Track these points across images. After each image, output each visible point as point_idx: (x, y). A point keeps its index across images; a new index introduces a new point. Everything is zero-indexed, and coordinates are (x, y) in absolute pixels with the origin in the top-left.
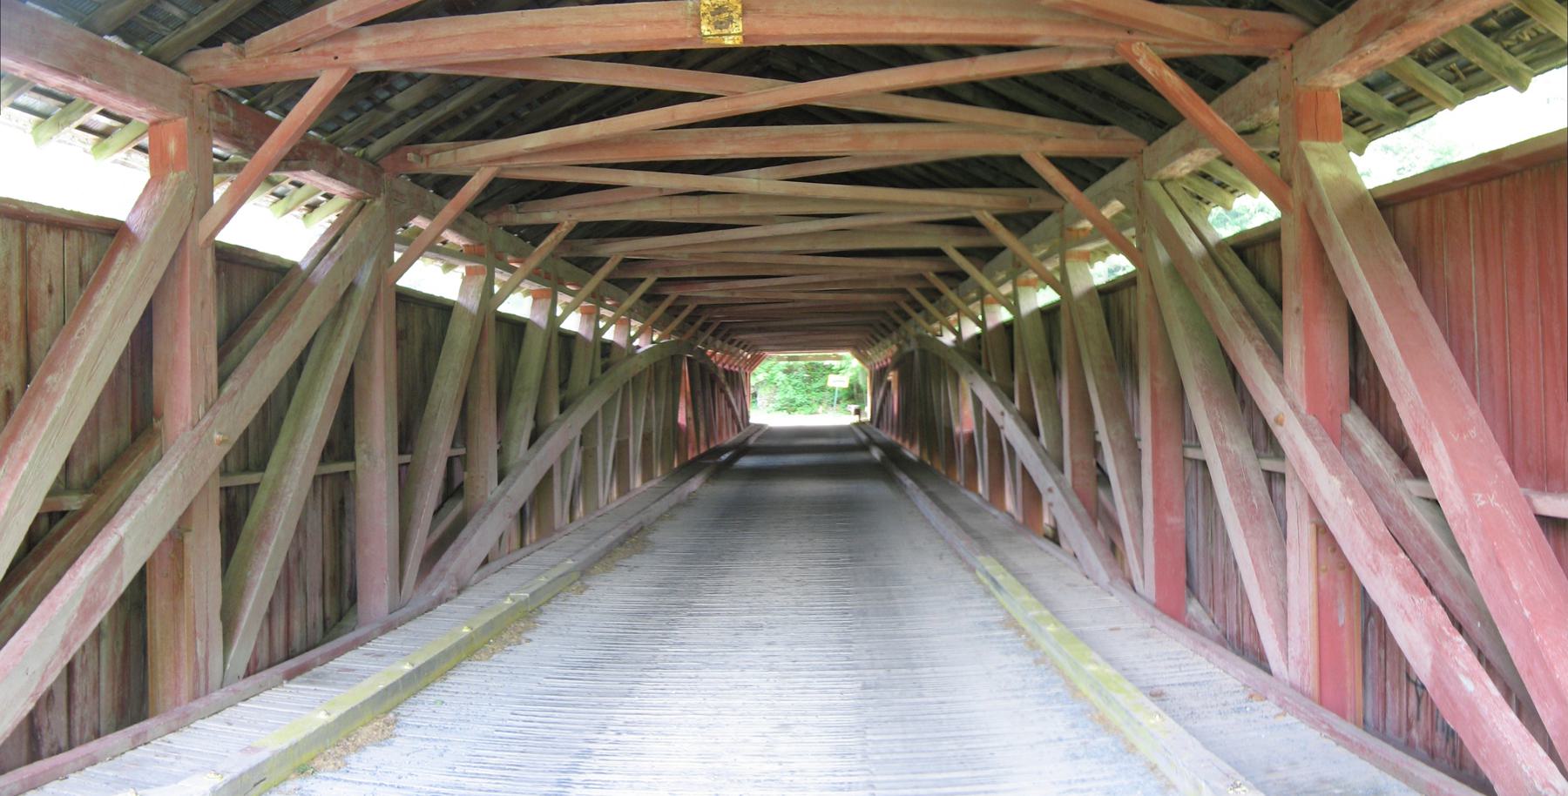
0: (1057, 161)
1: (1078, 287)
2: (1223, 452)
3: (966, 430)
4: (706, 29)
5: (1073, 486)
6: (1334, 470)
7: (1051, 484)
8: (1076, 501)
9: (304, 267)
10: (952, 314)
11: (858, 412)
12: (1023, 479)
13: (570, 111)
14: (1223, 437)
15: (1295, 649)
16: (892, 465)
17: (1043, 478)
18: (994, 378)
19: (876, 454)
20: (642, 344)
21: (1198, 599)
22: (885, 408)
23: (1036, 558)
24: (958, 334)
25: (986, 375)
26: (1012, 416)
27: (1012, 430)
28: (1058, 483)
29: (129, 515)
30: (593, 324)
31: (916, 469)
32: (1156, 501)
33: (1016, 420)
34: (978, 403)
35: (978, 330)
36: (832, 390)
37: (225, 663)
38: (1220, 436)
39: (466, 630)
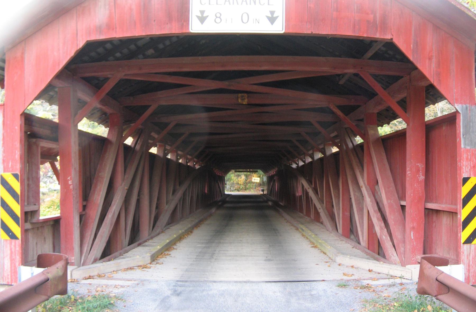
0: (319, 122)
1: (328, 153)
2: (354, 195)
3: (300, 194)
4: (240, 101)
5: (326, 207)
6: (370, 197)
7: (320, 207)
8: (326, 211)
9: (133, 146)
10: (296, 158)
11: (263, 191)
12: (314, 209)
13: (132, 55)
14: (355, 192)
15: (364, 239)
16: (276, 207)
17: (318, 206)
18: (307, 178)
19: (270, 203)
20: (197, 167)
21: (354, 235)
22: (273, 189)
23: (316, 227)
24: (298, 164)
25: (305, 177)
26: (311, 189)
27: (311, 194)
28: (322, 207)
29: (114, 204)
30: (186, 160)
31: (284, 208)
32: (343, 208)
33: (313, 190)
34: (303, 186)
35: (303, 164)
36: (254, 183)
37: (125, 240)
38: (354, 190)
39: (175, 236)
